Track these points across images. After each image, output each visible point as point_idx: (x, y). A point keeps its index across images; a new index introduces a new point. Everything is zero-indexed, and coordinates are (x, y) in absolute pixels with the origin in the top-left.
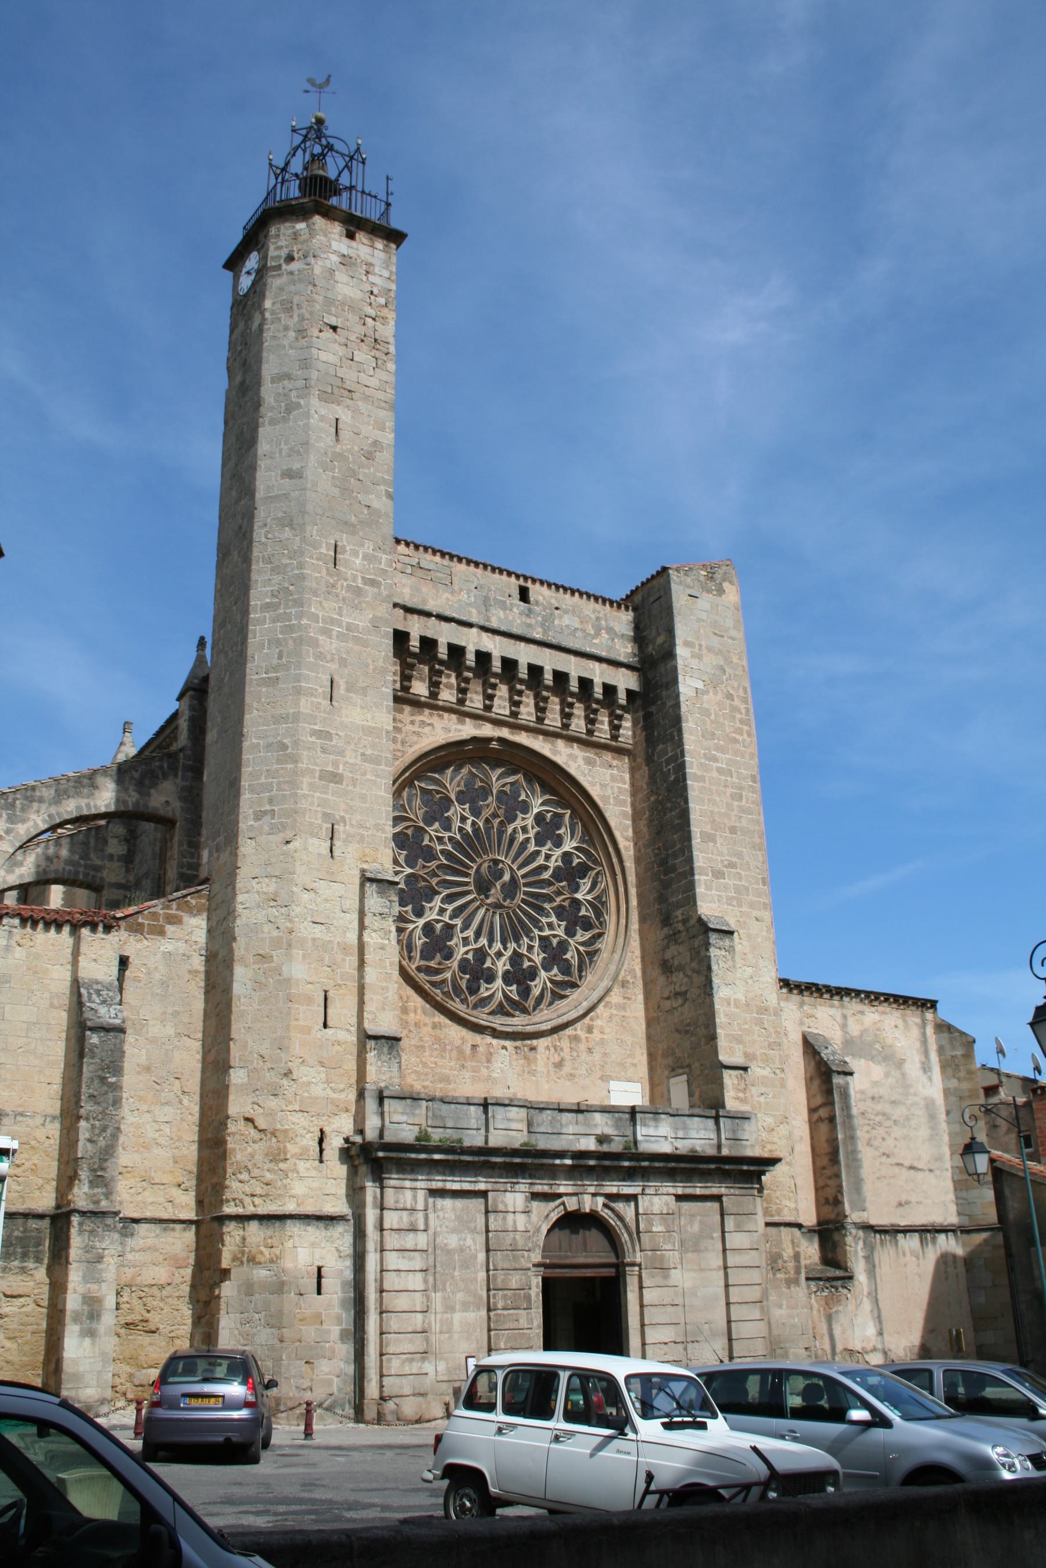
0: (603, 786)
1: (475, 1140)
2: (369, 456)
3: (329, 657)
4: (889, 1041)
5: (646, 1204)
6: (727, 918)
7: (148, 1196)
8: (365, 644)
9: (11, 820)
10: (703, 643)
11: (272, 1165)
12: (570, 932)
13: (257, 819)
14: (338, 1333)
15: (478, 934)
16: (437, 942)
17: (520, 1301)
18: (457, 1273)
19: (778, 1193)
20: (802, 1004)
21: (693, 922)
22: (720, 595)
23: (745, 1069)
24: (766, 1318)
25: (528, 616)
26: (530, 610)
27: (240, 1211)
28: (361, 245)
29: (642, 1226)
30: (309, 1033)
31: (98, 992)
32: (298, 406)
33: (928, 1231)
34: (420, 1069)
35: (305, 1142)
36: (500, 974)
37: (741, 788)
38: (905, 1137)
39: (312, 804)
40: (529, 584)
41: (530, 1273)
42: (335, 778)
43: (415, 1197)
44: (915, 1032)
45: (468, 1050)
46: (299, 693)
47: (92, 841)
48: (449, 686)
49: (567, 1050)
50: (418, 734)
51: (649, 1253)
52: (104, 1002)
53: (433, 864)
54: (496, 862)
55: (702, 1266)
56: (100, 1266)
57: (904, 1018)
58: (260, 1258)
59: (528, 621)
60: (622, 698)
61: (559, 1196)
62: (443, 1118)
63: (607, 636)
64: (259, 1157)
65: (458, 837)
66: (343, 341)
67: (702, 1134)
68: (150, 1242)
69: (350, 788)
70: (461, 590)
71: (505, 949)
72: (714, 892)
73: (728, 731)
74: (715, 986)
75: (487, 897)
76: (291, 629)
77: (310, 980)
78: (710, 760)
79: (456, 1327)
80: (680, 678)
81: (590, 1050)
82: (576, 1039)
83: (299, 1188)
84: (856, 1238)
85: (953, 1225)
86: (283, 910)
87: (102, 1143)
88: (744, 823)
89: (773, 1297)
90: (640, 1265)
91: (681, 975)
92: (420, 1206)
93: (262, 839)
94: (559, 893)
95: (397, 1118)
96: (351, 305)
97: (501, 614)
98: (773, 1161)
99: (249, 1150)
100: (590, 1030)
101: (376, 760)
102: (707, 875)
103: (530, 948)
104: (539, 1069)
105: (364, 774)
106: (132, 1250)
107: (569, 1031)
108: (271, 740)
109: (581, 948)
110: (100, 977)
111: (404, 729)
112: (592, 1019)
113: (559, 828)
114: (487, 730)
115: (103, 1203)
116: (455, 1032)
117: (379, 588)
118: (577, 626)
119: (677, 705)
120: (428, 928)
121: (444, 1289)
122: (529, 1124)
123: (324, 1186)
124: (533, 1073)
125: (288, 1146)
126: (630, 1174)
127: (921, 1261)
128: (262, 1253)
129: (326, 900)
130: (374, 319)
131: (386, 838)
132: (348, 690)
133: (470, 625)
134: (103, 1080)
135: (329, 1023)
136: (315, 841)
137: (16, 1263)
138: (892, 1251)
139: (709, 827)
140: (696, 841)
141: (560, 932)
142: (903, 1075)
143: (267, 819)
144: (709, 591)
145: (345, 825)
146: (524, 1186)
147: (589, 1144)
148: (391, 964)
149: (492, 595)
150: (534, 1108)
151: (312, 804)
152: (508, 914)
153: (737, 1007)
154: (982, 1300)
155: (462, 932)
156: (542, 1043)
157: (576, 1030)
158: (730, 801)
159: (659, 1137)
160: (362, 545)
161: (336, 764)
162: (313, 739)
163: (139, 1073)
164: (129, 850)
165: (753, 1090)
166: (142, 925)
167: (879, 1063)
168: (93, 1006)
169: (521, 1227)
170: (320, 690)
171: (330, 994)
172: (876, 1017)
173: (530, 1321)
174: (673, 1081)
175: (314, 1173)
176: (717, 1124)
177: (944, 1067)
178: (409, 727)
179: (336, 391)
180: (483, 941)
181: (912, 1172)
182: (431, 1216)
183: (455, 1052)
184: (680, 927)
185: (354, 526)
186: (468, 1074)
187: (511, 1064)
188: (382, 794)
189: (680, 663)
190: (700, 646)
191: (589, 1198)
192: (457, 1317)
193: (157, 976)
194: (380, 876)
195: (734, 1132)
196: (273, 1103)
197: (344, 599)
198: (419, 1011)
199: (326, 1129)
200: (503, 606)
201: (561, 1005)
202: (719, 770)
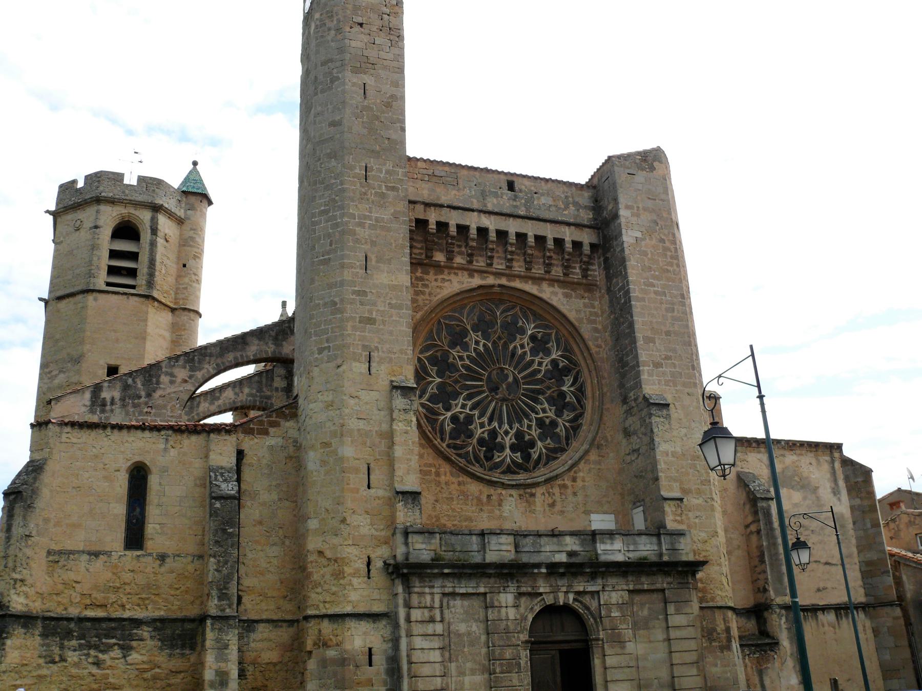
0: (578, 311)
1: (477, 559)
3: (363, 241)
4: (805, 475)
5: (606, 597)
6: (665, 396)
7: (264, 606)
8: (388, 230)
10: (640, 206)
11: (336, 582)
12: (559, 413)
13: (319, 353)
15: (491, 420)
16: (462, 427)
17: (513, 665)
18: (466, 650)
19: (712, 586)
21: (640, 399)
23: (681, 500)
24: (702, 673)
25: (514, 200)
26: (516, 196)
27: (317, 612)
29: (603, 613)
30: (357, 493)
31: (222, 475)
32: (338, 78)
33: (842, 608)
34: (450, 513)
35: (357, 565)
36: (508, 446)
37: (673, 304)
38: (821, 542)
39: (354, 340)
41: (519, 648)
42: (371, 321)
43: (433, 600)
44: (826, 467)
45: (485, 500)
46: (343, 267)
47: (264, 380)
48: (461, 253)
49: (557, 494)
50: (441, 288)
52: (225, 480)
53: (457, 375)
54: (502, 369)
55: (652, 639)
56: (226, 651)
57: (816, 457)
58: (329, 643)
60: (586, 249)
61: (541, 594)
62: (453, 545)
64: (328, 577)
65: (474, 355)
66: (367, 31)
67: (648, 547)
68: (265, 635)
69: (381, 327)
70: (465, 187)
71: (511, 428)
73: (661, 264)
74: (656, 444)
75: (497, 394)
76: (336, 225)
78: (648, 286)
79: (467, 686)
80: (624, 231)
81: (575, 494)
82: (564, 486)
83: (354, 596)
84: (780, 616)
85: (862, 603)
86: (338, 412)
87: (225, 571)
89: (710, 659)
90: (603, 640)
91: (636, 437)
92: (437, 604)
93: (324, 366)
94: (549, 388)
95: (418, 546)
97: (495, 201)
98: (704, 563)
99: (322, 572)
100: (574, 480)
101: (400, 307)
103: (529, 427)
104: (537, 509)
105: (391, 316)
106: (254, 640)
107: (559, 482)
108: (327, 300)
109: (567, 424)
110: (224, 464)
112: (575, 472)
113: (548, 343)
114: (491, 280)
115: (228, 610)
116: (474, 488)
118: (551, 203)
119: (623, 250)
120: (454, 419)
121: (457, 660)
122: (516, 546)
123: (361, 593)
124: (533, 512)
125: (346, 568)
126: (593, 576)
127: (837, 630)
128: (331, 640)
129: (367, 403)
132: (377, 262)
133: (473, 210)
134: (224, 531)
135: (371, 485)
136: (358, 364)
137: (178, 651)
138: (814, 624)
140: (640, 343)
141: (551, 414)
142: (818, 498)
143: (326, 352)
144: (643, 170)
146: (512, 587)
147: (562, 558)
148: (413, 443)
149: (487, 189)
150: (518, 535)
151: (354, 340)
152: (512, 405)
153: (673, 456)
154: (887, 657)
155: (479, 418)
156: (539, 491)
159: (614, 551)
160: (385, 164)
161: (370, 312)
162: (354, 297)
163: (255, 525)
164: (288, 384)
165: (691, 514)
167: (798, 490)
168: (217, 483)
169: (511, 617)
171: (372, 466)
172: (795, 458)
173: (521, 680)
174: (635, 511)
175: (364, 586)
176: (659, 540)
177: (850, 490)
178: (434, 284)
179: (363, 65)
180: (495, 424)
181: (827, 567)
182: (446, 612)
184: (633, 404)
185: (379, 152)
186: (485, 515)
187: (516, 506)
189: (623, 220)
190: (638, 207)
191: (563, 594)
192: (467, 679)
193: (264, 462)
194: (403, 384)
195: (672, 544)
196: (336, 541)
197: (373, 202)
199: (372, 556)
200: (496, 195)
201: (554, 464)
202: (656, 293)
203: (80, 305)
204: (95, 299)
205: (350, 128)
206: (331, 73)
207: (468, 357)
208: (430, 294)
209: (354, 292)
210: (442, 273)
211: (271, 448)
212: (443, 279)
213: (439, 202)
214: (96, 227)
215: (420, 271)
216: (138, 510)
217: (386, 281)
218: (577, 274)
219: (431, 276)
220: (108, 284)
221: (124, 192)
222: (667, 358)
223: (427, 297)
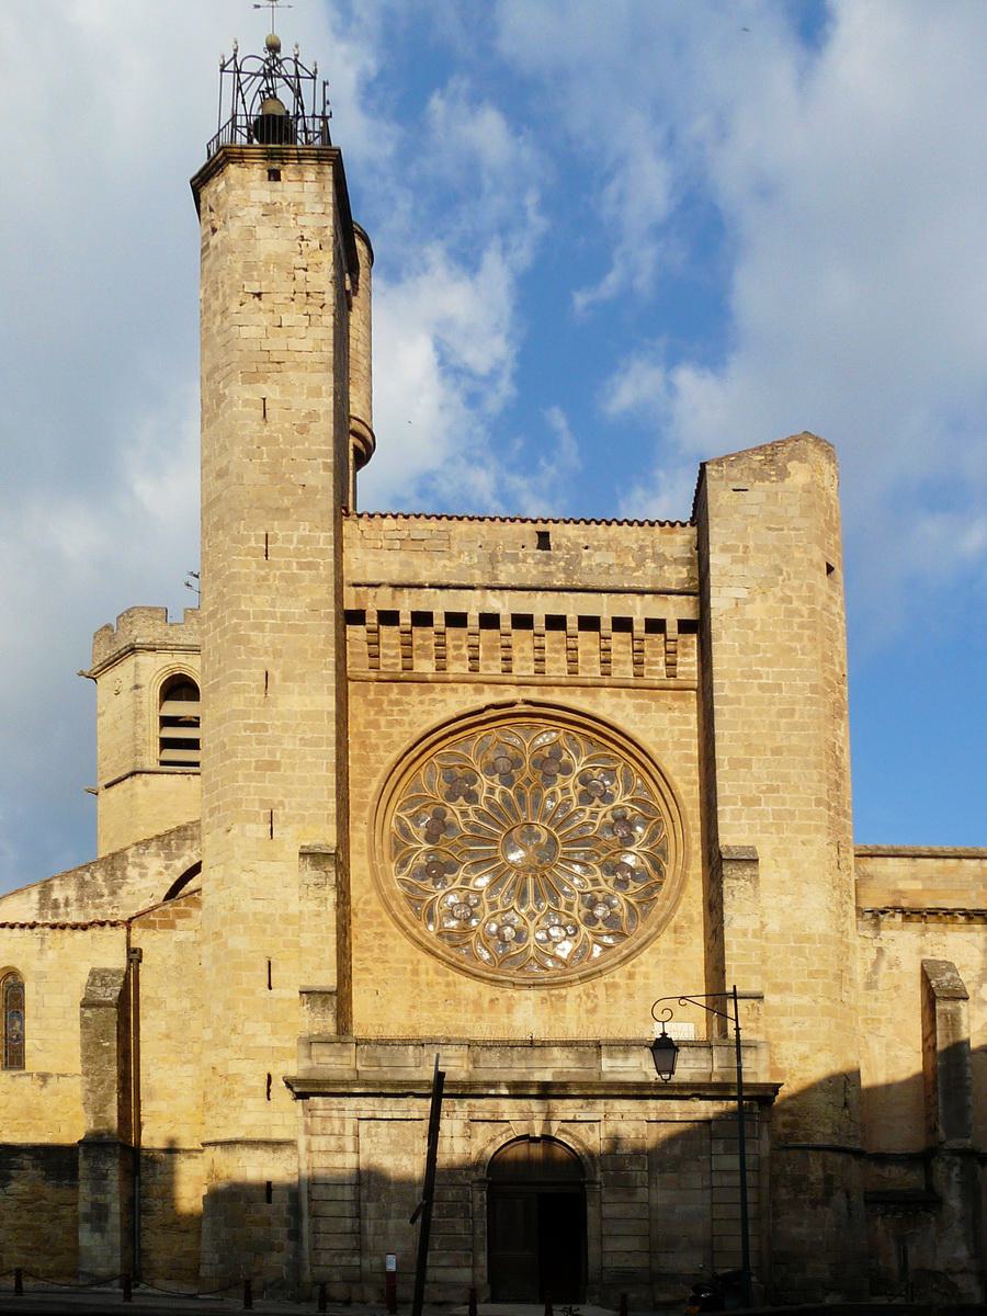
0: (659, 732)
2: (303, 430)
8: (303, 629)
9: (169, 857)
10: (751, 544)
13: (211, 816)
14: (286, 1232)
19: (809, 1119)
20: (923, 932)
22: (783, 480)
28: (287, 184)
39: (249, 794)
40: (550, 527)
43: (343, 1126)
45: (486, 1003)
50: (429, 713)
51: (611, 1173)
56: (104, 1182)
59: (547, 569)
63: (653, 565)
66: (269, 306)
70: (461, 552)
72: (743, 821)
77: (251, 949)
78: (749, 677)
81: (631, 996)
87: (101, 1092)
88: (795, 741)
92: (349, 1130)
96: (279, 262)
97: (512, 568)
100: (631, 976)
101: (317, 743)
102: (735, 804)
104: (568, 1016)
107: (606, 979)
111: (412, 711)
117: (317, 569)
121: (378, 1200)
130: (306, 270)
131: (328, 815)
132: (285, 679)
135: (272, 985)
137: (66, 1182)
139: (742, 752)
145: (284, 808)
151: (249, 794)
156: (572, 992)
157: (613, 977)
158: (775, 719)
161: (272, 753)
163: (160, 1039)
166: (153, 922)
170: (253, 685)
178: (419, 708)
183: (471, 1006)
185: (287, 510)
188: (324, 773)
192: (392, 1223)
193: (171, 962)
198: (431, 972)
200: (514, 559)
202: (761, 687)
203: (129, 793)
204: (146, 784)
205: (240, 477)
206: (217, 389)
207: (476, 811)
208: (411, 724)
209: (247, 727)
210: (431, 690)
211: (179, 944)
212: (434, 700)
213: (417, 581)
214: (137, 687)
215: (396, 690)
216: (18, 1024)
217: (296, 708)
218: (660, 673)
219: (414, 698)
220: (163, 763)
221: (167, 634)
222: (772, 789)
223: (407, 728)
